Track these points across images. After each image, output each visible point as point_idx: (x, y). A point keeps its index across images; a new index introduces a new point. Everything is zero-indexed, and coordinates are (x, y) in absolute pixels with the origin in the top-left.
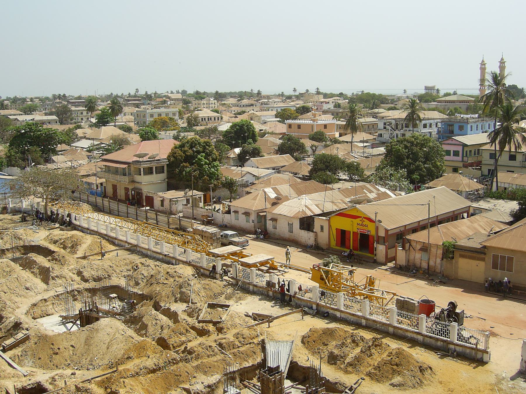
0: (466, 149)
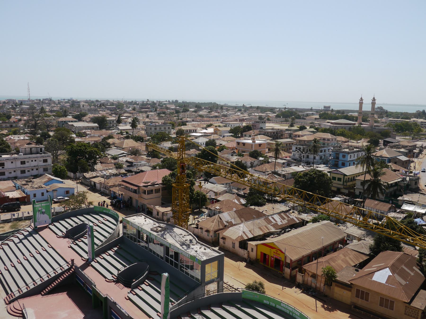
0: (346, 177)
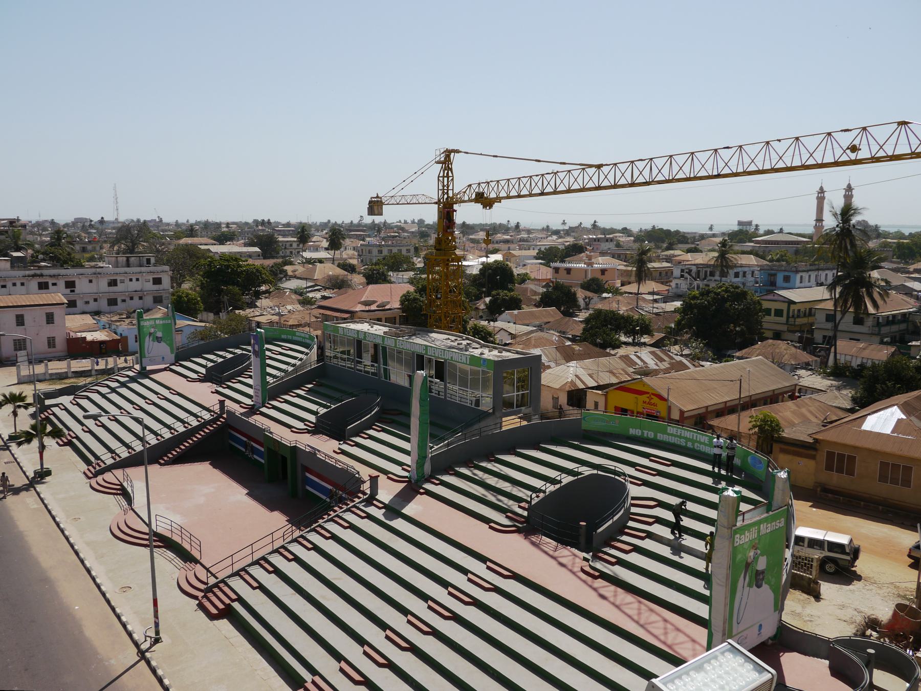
0: (792, 307)
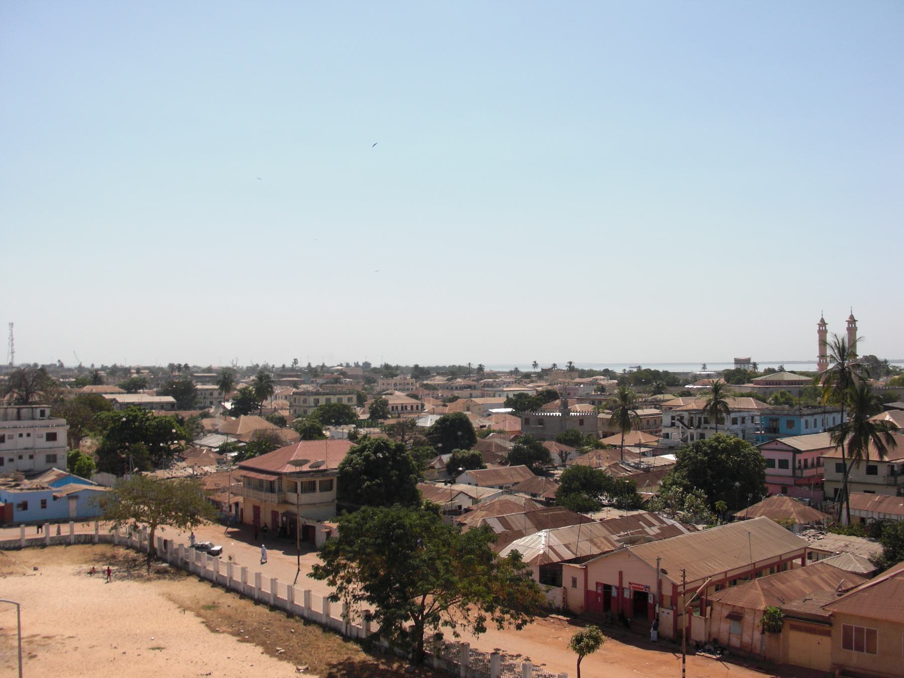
0: (798, 457)
